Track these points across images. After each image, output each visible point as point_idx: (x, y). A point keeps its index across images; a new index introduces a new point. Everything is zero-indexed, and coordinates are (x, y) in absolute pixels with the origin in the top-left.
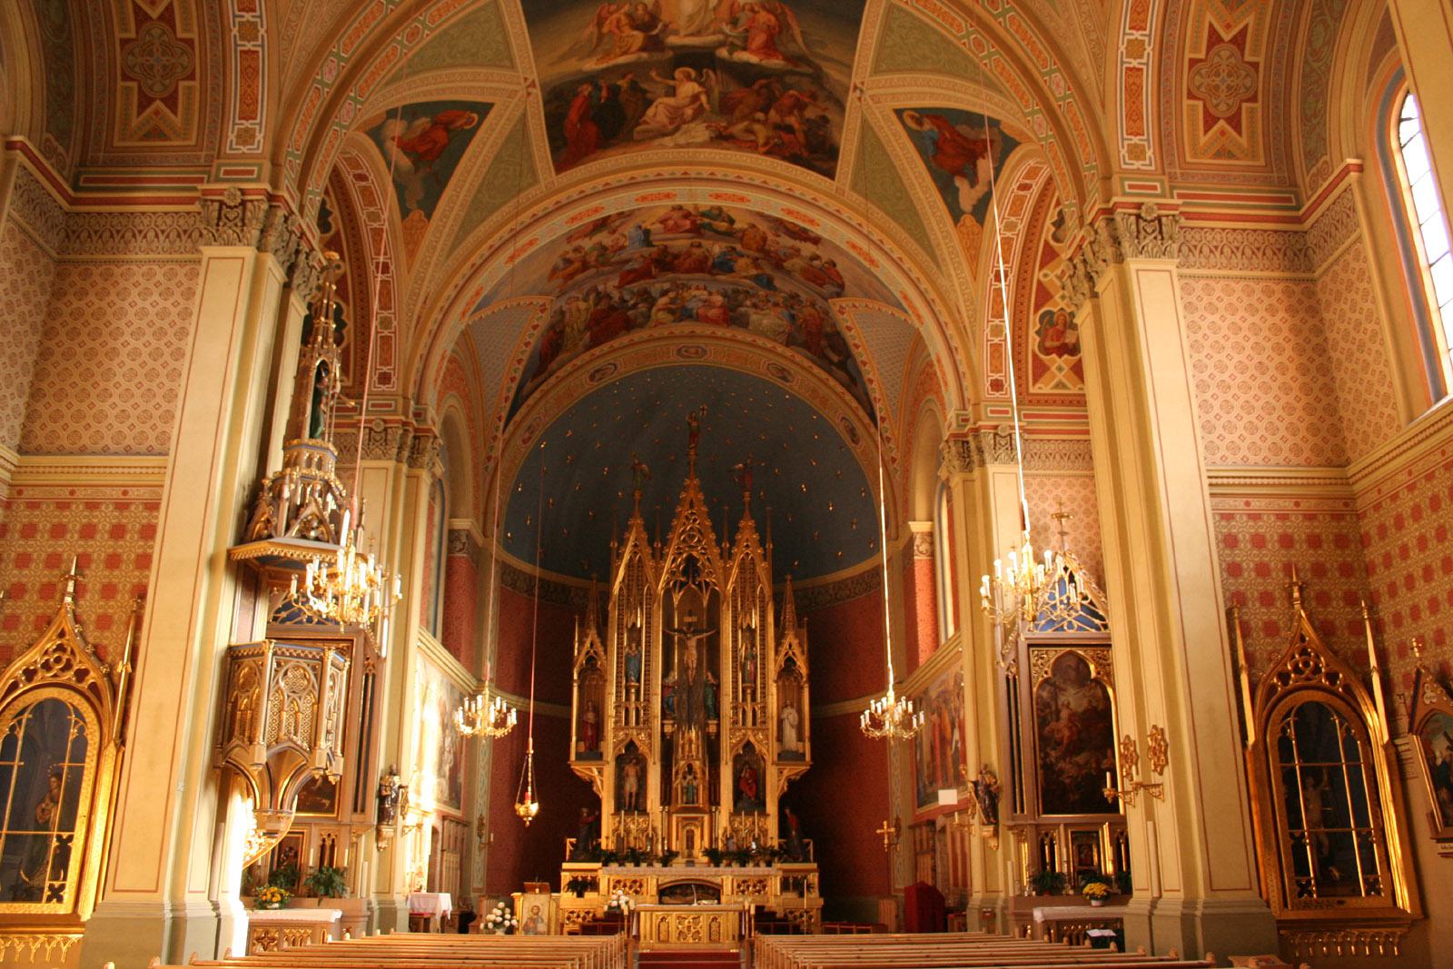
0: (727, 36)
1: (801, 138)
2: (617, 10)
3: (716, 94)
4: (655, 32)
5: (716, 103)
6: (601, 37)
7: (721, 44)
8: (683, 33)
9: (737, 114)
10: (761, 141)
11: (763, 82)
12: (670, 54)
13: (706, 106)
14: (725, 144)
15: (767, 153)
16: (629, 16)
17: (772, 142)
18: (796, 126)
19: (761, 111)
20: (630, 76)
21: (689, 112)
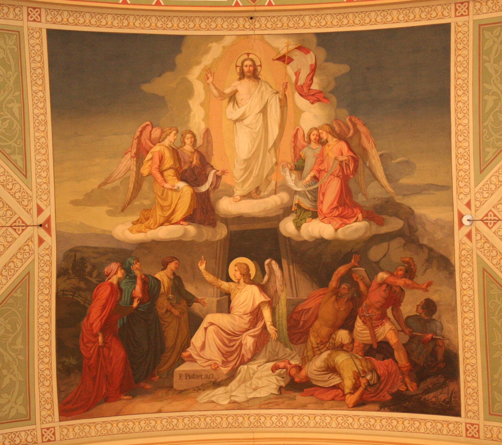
0: (293, 193)
1: (401, 356)
2: (159, 140)
3: (282, 309)
4: (204, 188)
5: (284, 322)
6: (139, 180)
7: (287, 211)
8: (239, 192)
9: (313, 340)
10: (348, 383)
11: (342, 269)
12: (222, 232)
13: (271, 329)
14: (300, 398)
15: (360, 404)
16: (175, 152)
17: (363, 381)
18: (393, 340)
19: (342, 327)
20: (172, 266)
21: (249, 341)
